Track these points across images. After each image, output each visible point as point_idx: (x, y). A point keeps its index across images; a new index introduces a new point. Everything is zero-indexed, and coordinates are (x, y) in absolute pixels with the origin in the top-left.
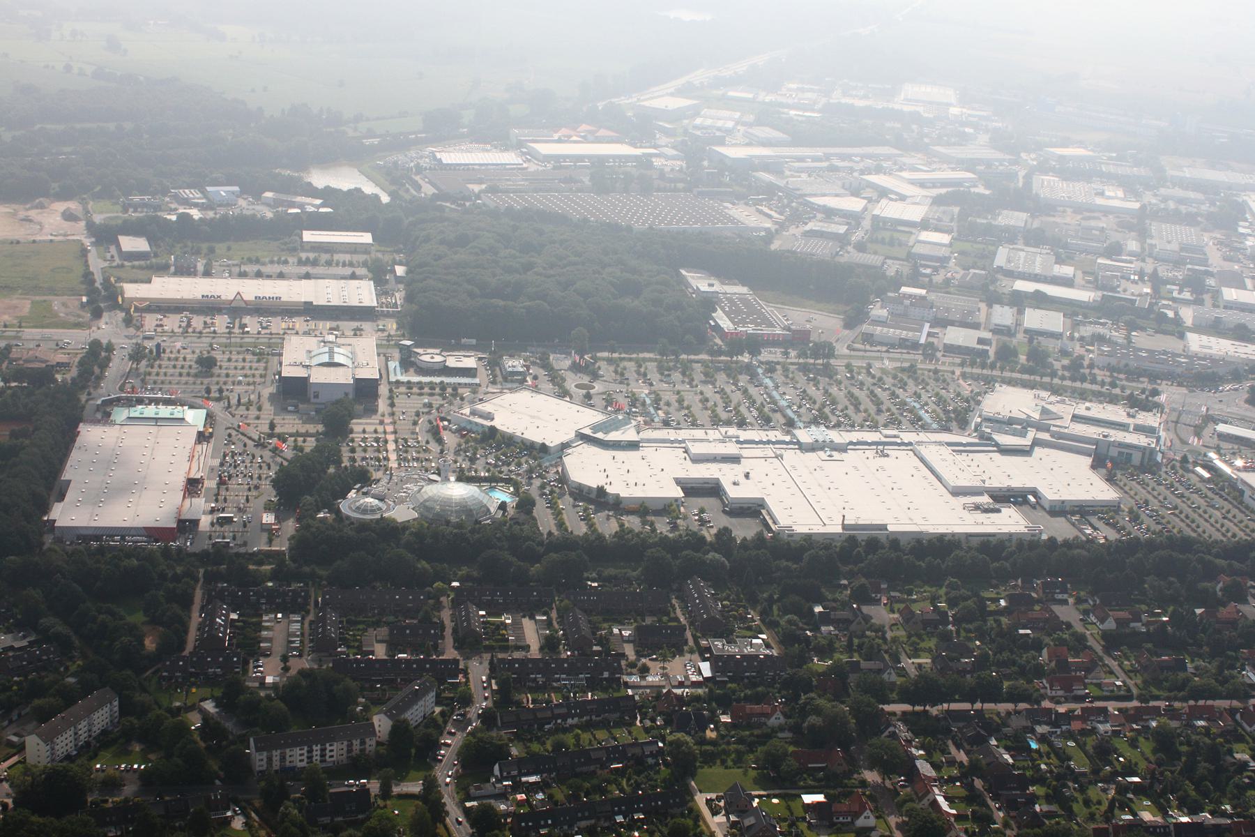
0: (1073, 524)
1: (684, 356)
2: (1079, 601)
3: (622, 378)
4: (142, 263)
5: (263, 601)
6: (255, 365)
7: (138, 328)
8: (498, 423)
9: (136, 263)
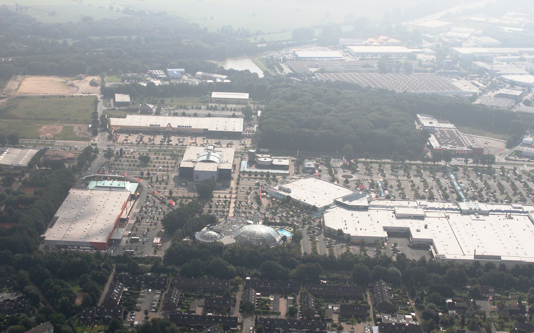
1: (407, 161)
5: (143, 282)
8: (292, 195)
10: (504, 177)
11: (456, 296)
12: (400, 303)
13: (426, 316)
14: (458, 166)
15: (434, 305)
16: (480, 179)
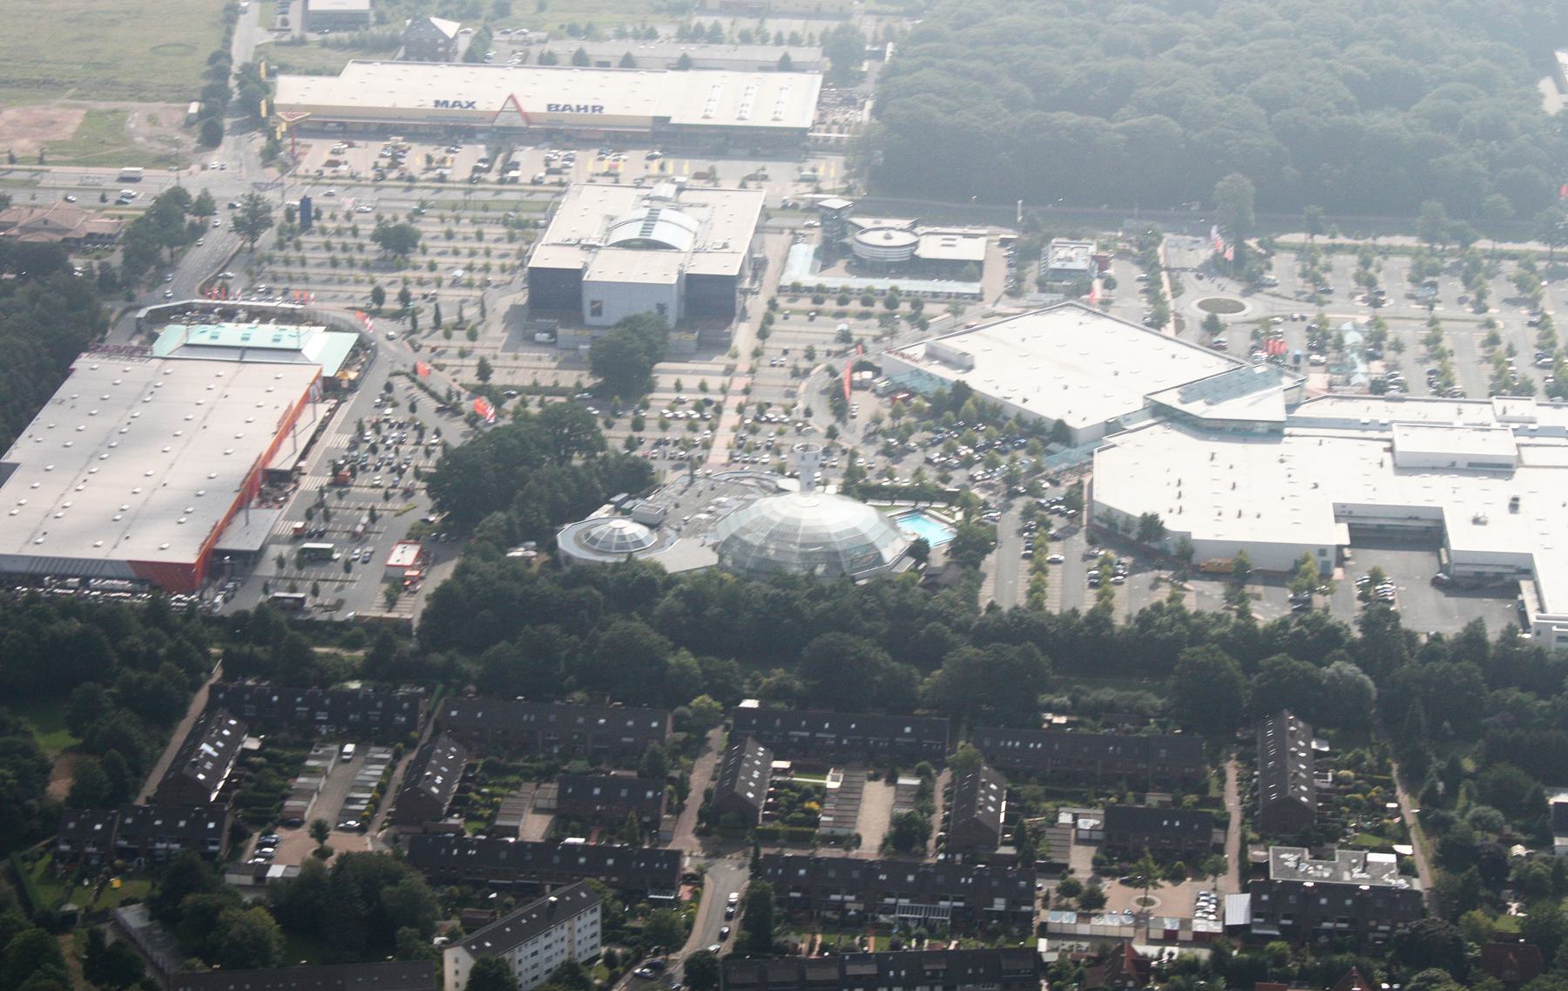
1: (1484, 244)
4: (344, 36)
5: (322, 716)
6: (504, 247)
7: (285, 168)
9: (332, 36)
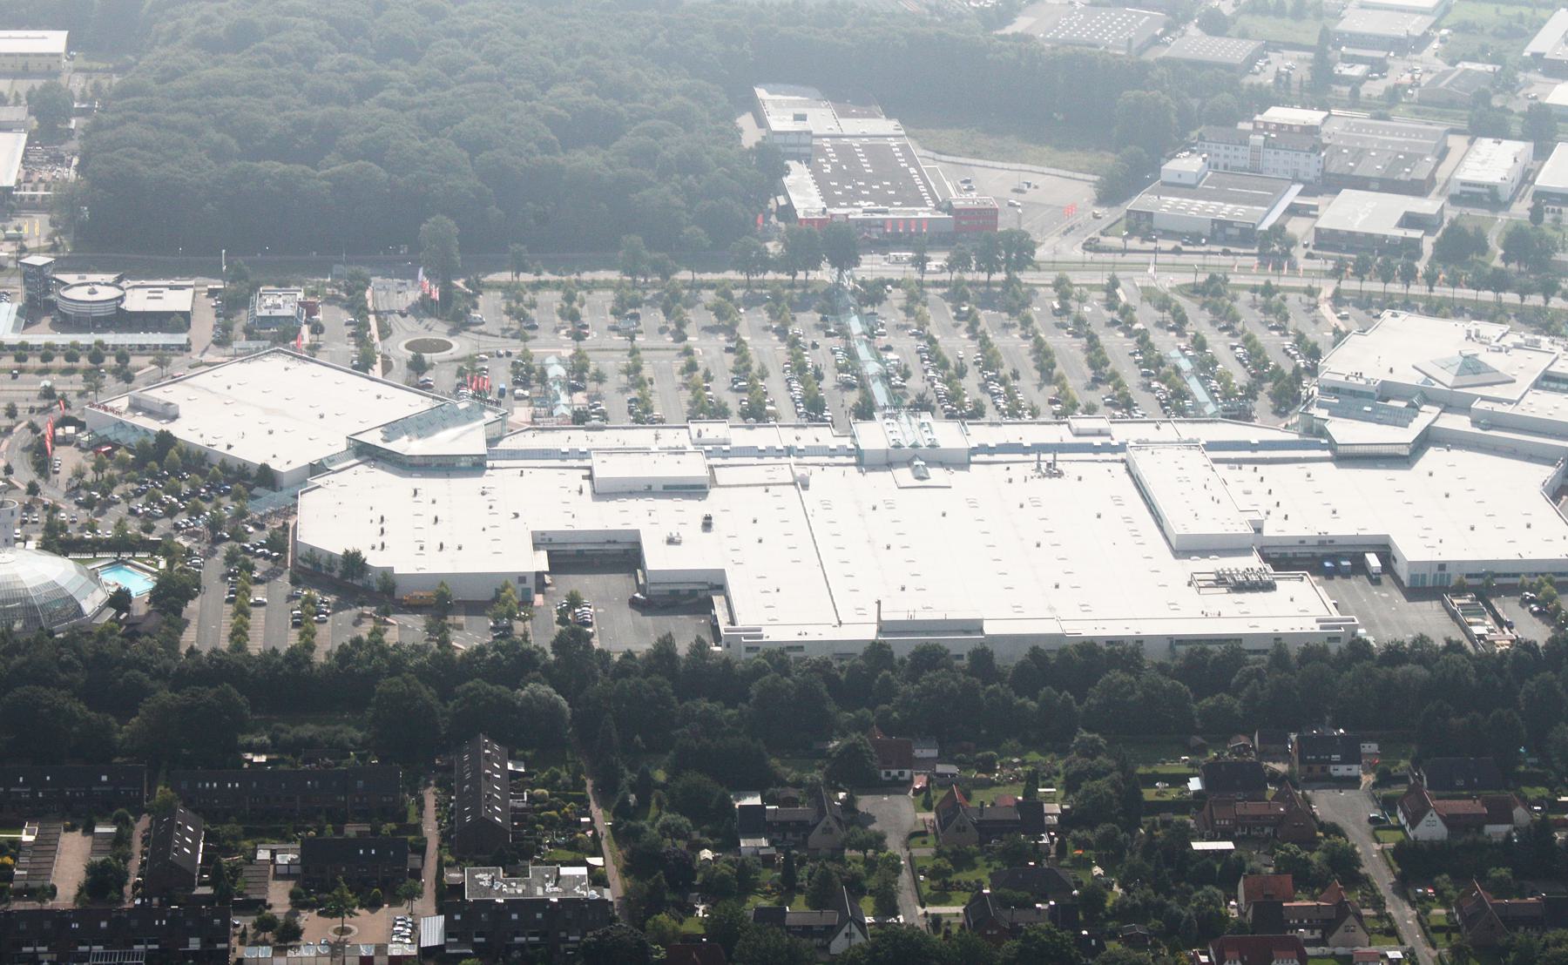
0: (1454, 616)
1: (684, 275)
2: (1384, 779)
3: (524, 327)
8: (178, 430)
10: (1065, 319)
11: (782, 783)
12: (551, 824)
13: (638, 863)
14: (890, 282)
15: (684, 821)
16: (967, 330)
